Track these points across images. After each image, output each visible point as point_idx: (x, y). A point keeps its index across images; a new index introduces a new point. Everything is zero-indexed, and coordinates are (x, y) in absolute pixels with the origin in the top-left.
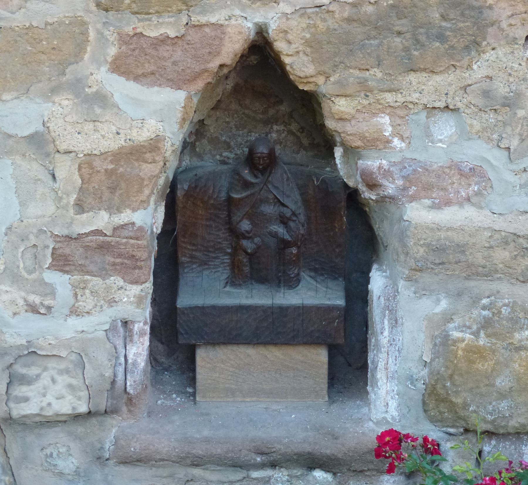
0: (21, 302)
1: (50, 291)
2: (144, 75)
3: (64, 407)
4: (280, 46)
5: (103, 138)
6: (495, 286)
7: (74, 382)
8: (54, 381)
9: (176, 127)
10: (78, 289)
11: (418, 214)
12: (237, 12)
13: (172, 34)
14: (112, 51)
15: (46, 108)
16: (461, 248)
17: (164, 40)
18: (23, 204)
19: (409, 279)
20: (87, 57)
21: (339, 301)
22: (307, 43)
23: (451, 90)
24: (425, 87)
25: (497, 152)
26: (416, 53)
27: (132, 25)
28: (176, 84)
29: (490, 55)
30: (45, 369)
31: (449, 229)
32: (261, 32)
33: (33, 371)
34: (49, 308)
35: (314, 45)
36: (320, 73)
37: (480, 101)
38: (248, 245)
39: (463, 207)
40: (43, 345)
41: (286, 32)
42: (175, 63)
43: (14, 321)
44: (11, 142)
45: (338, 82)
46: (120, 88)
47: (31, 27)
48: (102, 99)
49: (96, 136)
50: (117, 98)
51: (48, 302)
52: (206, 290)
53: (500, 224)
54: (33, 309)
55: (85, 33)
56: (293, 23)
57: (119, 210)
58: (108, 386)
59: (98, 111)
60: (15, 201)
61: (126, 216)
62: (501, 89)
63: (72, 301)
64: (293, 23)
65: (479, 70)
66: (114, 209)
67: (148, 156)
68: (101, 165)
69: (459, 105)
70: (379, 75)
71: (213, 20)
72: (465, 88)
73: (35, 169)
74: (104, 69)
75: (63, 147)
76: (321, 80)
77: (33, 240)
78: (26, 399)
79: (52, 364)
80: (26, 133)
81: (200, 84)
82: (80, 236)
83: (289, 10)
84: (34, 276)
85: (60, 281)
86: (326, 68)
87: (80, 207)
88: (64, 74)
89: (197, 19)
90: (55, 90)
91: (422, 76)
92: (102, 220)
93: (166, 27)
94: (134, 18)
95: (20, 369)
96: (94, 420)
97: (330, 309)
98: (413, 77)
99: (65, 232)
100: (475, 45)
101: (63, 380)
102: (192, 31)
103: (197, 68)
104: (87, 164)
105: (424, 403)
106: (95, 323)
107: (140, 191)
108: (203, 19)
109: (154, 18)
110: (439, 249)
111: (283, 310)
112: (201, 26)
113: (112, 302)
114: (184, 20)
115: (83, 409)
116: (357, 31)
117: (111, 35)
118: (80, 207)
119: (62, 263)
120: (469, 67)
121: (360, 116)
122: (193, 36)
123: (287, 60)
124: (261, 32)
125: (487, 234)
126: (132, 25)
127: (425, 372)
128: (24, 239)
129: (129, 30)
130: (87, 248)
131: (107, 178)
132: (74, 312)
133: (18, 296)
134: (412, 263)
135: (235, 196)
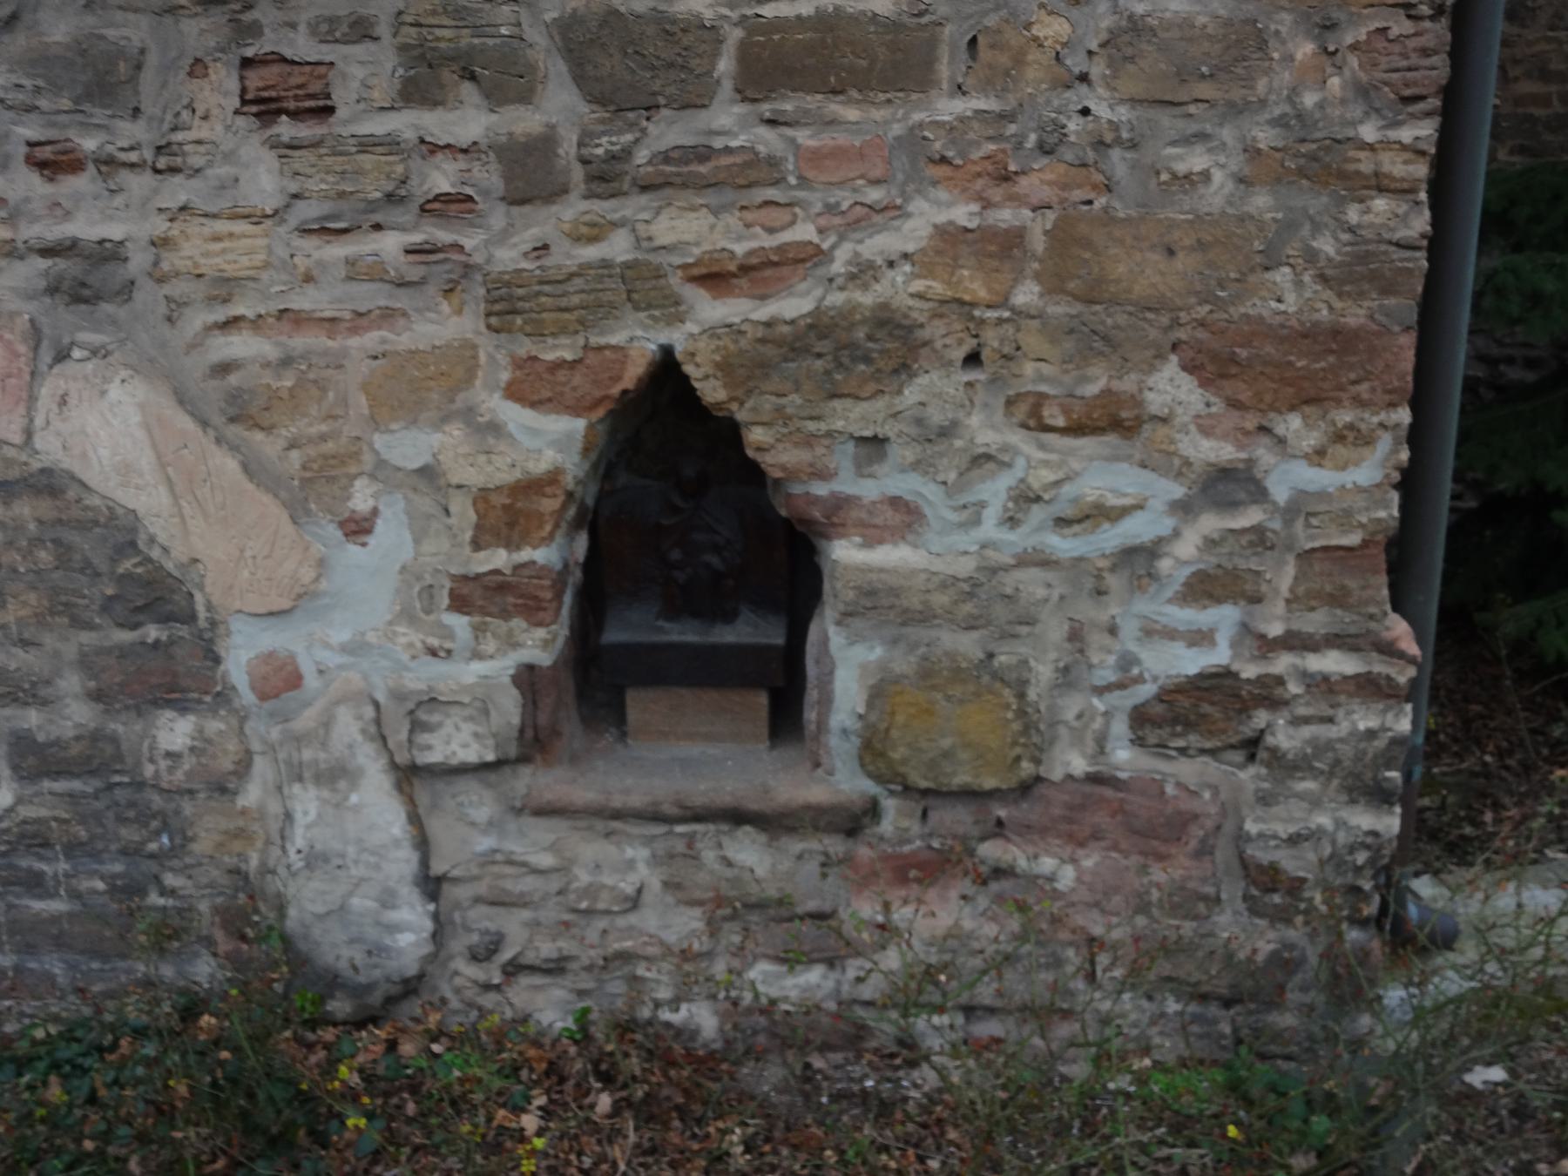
0: (419, 645)
1: (449, 634)
2: (541, 402)
3: (471, 755)
4: (688, 369)
5: (500, 471)
6: (934, 633)
7: (480, 730)
8: (457, 728)
9: (576, 458)
10: (479, 630)
11: (844, 552)
12: (639, 333)
13: (569, 356)
14: (505, 376)
15: (436, 439)
16: (894, 592)
17: (560, 365)
18: (417, 541)
19: (838, 623)
20: (478, 383)
21: (779, 640)
22: (718, 365)
23: (880, 417)
24: (852, 417)
25: (933, 487)
26: (839, 377)
27: (525, 347)
28: (575, 410)
29: (923, 380)
30: (448, 716)
31: (881, 570)
32: (667, 351)
33: (435, 718)
34: (449, 652)
35: (725, 368)
36: (732, 399)
37: (913, 431)
38: (681, 576)
39: (620, 719)
40: (444, 691)
41: (693, 355)
42: (574, 389)
43: (413, 664)
44: (400, 475)
45: (754, 409)
46: (514, 415)
47: (417, 352)
48: (495, 428)
49: (490, 469)
50: (511, 427)
51: (448, 645)
52: (625, 629)
53: (938, 566)
54: (433, 652)
55: (475, 357)
56: (701, 345)
57: (518, 548)
58: (515, 734)
59: (491, 441)
60: (408, 537)
61: (526, 554)
62: (936, 417)
63: (473, 643)
64: (701, 345)
65: (911, 395)
66: (510, 545)
67: (548, 490)
68: (499, 500)
69: (890, 434)
70: (799, 401)
71: (614, 340)
72: (895, 415)
73: (426, 504)
74: (497, 395)
75: (455, 480)
76: (734, 406)
77: (429, 580)
78: (429, 747)
79: (454, 710)
80: (416, 465)
81: (600, 412)
82: (478, 577)
83: (695, 329)
84: (432, 617)
85: (460, 624)
86: (740, 393)
87: (477, 545)
88: (452, 401)
89: (595, 340)
90: (446, 419)
91: (848, 402)
92: (499, 559)
93: (562, 350)
94: (527, 340)
95: (422, 715)
96: (507, 770)
97: (769, 648)
98: (837, 404)
99: (462, 571)
100: (904, 369)
101: (468, 728)
102: (591, 354)
103: (598, 394)
104: (482, 497)
105: (861, 758)
106: (501, 667)
107: (540, 527)
108: (602, 341)
109: (550, 341)
110: (871, 593)
111: (715, 649)
112: (600, 349)
113: (516, 645)
114: (581, 342)
115: (490, 757)
116: (770, 351)
117: (502, 358)
118: (477, 545)
119: (460, 603)
120: (899, 392)
121: (780, 446)
122: (592, 359)
123: (696, 385)
124: (667, 351)
125: (923, 576)
126: (525, 347)
127: (858, 725)
128: (419, 578)
129: (522, 352)
130: (486, 588)
131: (505, 514)
132: (477, 655)
133: (416, 638)
134: (841, 607)
135: (665, 522)
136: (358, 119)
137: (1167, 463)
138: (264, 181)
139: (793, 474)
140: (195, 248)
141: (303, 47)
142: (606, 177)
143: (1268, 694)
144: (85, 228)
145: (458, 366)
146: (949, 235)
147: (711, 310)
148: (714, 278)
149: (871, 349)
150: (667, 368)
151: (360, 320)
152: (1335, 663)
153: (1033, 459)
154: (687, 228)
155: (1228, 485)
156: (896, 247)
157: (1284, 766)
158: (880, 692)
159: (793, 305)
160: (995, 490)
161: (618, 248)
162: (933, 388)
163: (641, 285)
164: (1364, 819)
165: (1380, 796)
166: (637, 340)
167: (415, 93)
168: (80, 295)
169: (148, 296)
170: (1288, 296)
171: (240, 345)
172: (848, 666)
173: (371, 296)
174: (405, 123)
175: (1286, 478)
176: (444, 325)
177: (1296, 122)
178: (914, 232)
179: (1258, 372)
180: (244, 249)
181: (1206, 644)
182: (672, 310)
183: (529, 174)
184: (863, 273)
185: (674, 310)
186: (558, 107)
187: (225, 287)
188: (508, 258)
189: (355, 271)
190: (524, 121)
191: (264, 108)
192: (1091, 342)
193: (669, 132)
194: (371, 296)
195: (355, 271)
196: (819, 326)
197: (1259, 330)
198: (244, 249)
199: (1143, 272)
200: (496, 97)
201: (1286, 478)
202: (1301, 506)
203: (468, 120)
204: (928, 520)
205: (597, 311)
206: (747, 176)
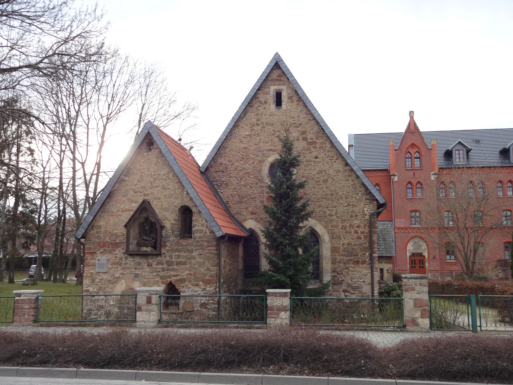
100: (185, 282)
136: (153, 266)
137: (200, 288)
138: (148, 270)
139: (262, 231)
140: (143, 274)
141: (151, 262)
142: (168, 270)
143: (207, 304)
144: (137, 273)
145: (158, 281)
146: (188, 274)
147: (174, 278)
148: (174, 276)
149: (183, 281)
150: (171, 282)
151: (153, 278)
152: (211, 302)
153: (193, 288)
154: (172, 273)
155: (204, 289)
156: (184, 274)
157: (209, 309)
158: (184, 304)
159: (178, 278)
160: (190, 290)
161: (168, 274)
162: (187, 283)
163: (169, 277)
164: (214, 313)
165: (214, 311)
166: (169, 280)
167: (157, 265)
168: (136, 277)
169: (140, 277)
170: (207, 277)
171: (145, 280)
172: (182, 302)
173: (154, 277)
174: (156, 267)
175: (208, 289)
176: (158, 279)
177: (207, 267)
178: (185, 273)
179: (207, 282)
180: (146, 274)
181: (204, 300)
182: (171, 278)
183: (163, 270)
184: (182, 276)
185: (171, 278)
186: (165, 266)
187: (145, 276)
188: (162, 275)
189: (153, 275)
190: (163, 266)
191: (148, 266)
192: (196, 280)
193: (172, 267)
194: (154, 277)
195: (153, 275)
196: (180, 279)
197: (206, 280)
198: (146, 274)
199: (199, 276)
200: (162, 265)
201: (208, 289)
202: (209, 291)
203: (160, 266)
204: (186, 291)
205: (167, 278)
206: (176, 270)
